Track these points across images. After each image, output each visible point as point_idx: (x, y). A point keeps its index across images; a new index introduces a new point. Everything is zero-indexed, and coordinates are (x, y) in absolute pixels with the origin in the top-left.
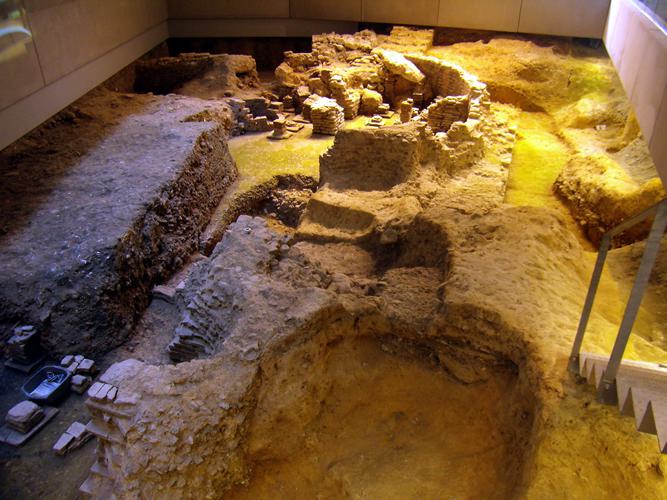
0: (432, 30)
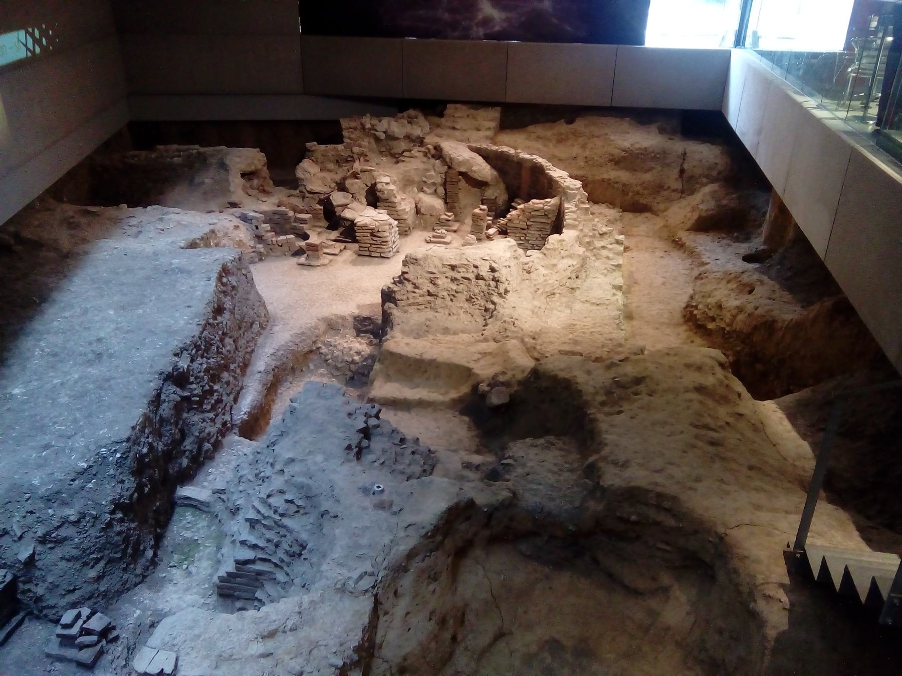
0: (499, 108)
